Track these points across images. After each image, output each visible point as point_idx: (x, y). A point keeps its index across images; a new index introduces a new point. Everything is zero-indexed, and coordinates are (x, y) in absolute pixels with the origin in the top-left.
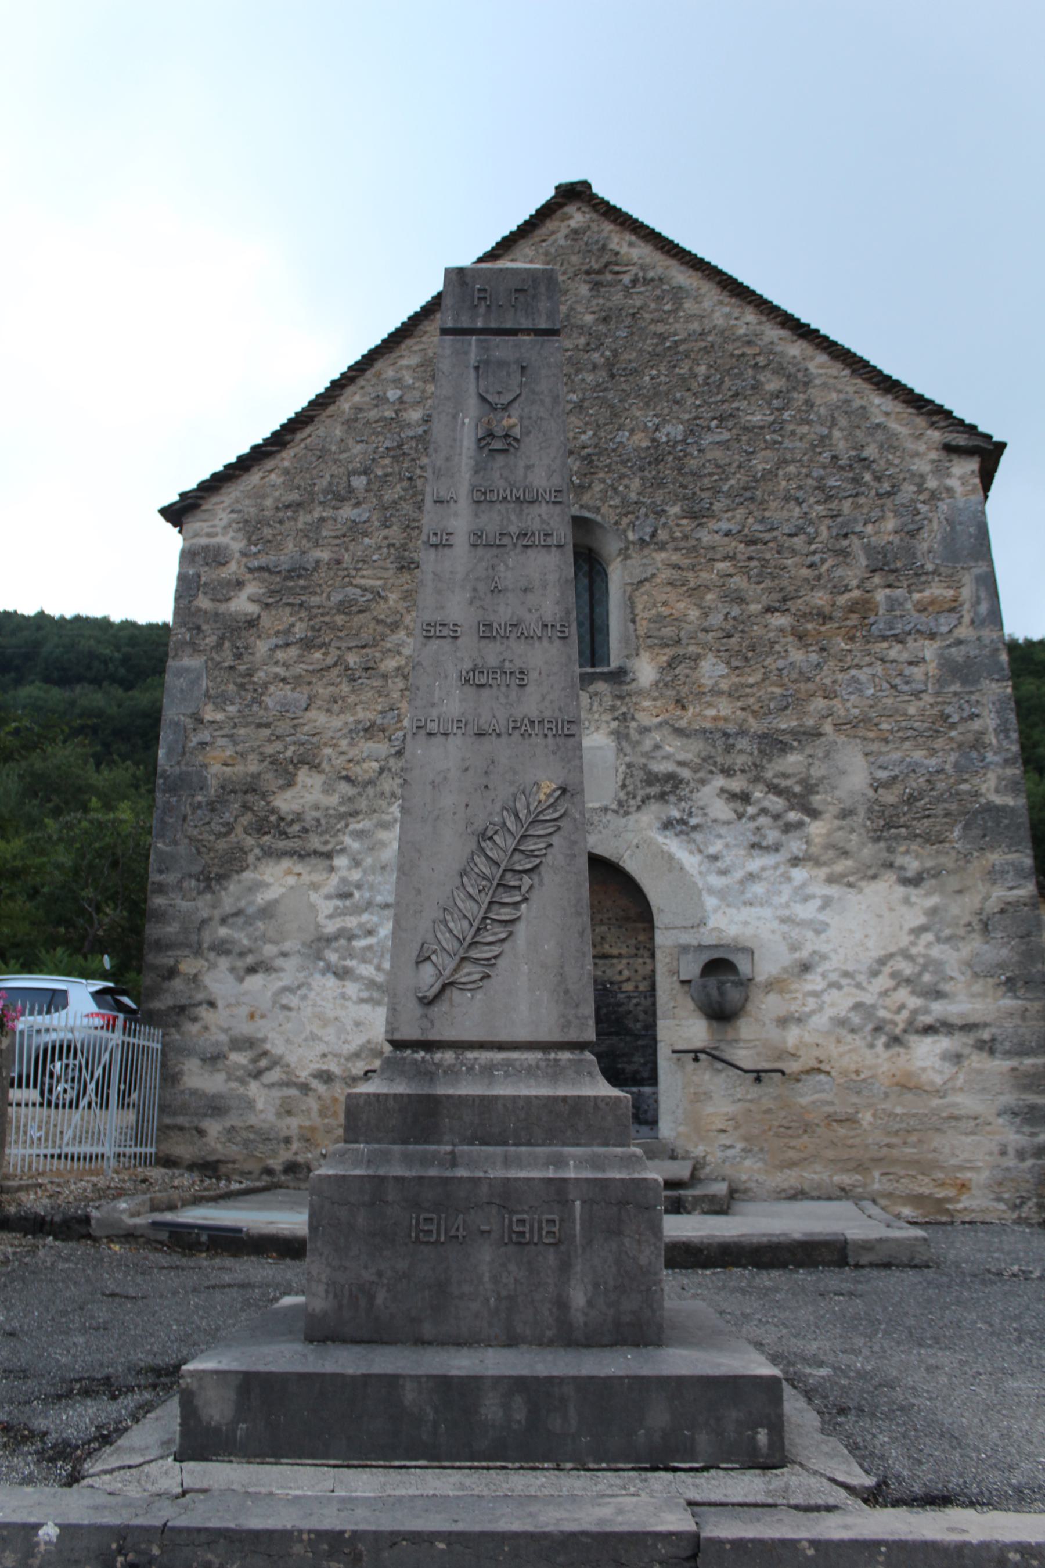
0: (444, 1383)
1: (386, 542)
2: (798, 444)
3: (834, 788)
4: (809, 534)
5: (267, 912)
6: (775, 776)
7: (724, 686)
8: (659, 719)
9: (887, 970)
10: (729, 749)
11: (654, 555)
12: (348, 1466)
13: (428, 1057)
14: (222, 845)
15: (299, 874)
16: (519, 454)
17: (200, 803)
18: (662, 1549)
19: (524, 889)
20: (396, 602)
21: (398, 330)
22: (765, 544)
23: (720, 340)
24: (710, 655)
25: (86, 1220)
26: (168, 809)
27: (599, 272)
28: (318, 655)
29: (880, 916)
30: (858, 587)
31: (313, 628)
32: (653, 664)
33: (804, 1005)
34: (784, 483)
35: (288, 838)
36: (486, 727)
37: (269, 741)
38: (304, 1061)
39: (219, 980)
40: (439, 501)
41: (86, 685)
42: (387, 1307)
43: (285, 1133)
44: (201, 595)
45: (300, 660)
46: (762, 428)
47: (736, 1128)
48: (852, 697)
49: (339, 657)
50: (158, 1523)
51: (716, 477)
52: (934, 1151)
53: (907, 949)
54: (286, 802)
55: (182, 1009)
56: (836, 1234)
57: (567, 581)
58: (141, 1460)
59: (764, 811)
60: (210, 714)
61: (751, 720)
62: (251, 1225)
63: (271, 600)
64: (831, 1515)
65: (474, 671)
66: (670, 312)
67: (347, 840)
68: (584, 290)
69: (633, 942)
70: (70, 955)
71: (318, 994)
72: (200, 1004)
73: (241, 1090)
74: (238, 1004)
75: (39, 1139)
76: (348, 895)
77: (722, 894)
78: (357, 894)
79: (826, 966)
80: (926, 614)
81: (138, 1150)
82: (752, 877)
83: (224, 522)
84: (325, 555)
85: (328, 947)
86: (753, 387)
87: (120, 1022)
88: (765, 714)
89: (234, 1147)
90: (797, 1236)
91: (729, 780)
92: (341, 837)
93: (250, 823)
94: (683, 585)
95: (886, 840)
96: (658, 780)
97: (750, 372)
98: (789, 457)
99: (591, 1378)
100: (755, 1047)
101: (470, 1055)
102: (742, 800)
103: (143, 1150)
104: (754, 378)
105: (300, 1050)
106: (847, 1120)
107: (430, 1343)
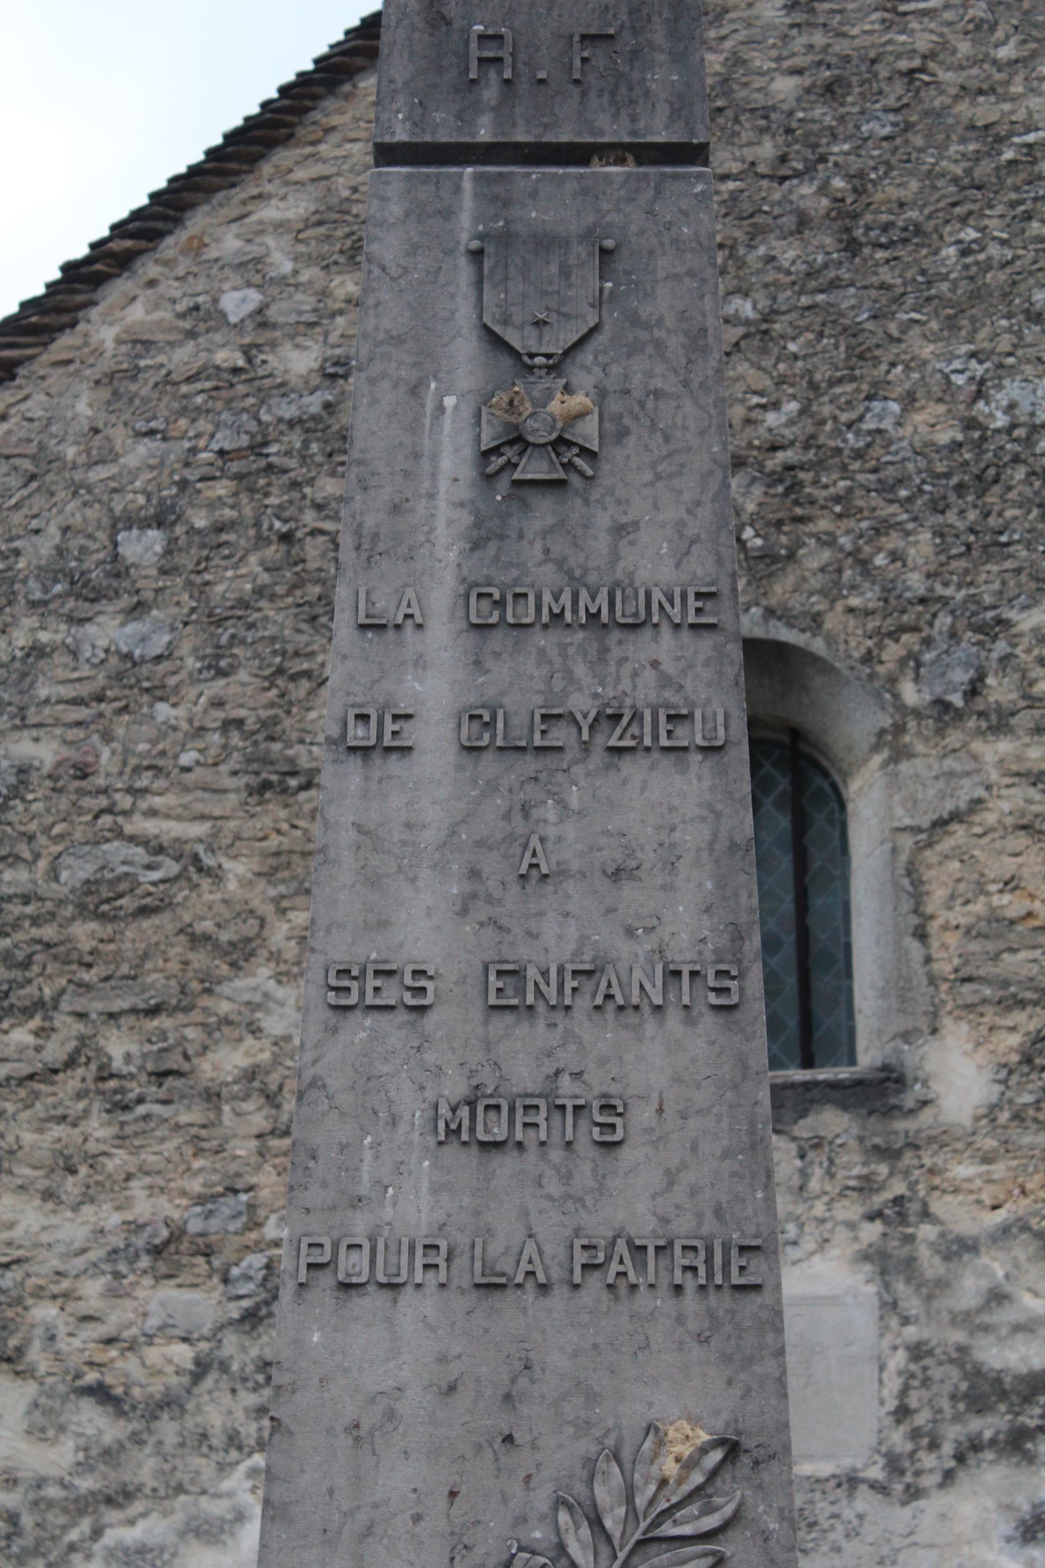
1: (220, 714)
8: (1000, 1216)
11: (977, 746)
16: (595, 494)
20: (246, 884)
21: (251, 124)
28: (21, 1035)
36: (505, 1265)
49: (82, 1039)
65: (472, 1104)
84: (44, 752)
96: (1004, 1395)
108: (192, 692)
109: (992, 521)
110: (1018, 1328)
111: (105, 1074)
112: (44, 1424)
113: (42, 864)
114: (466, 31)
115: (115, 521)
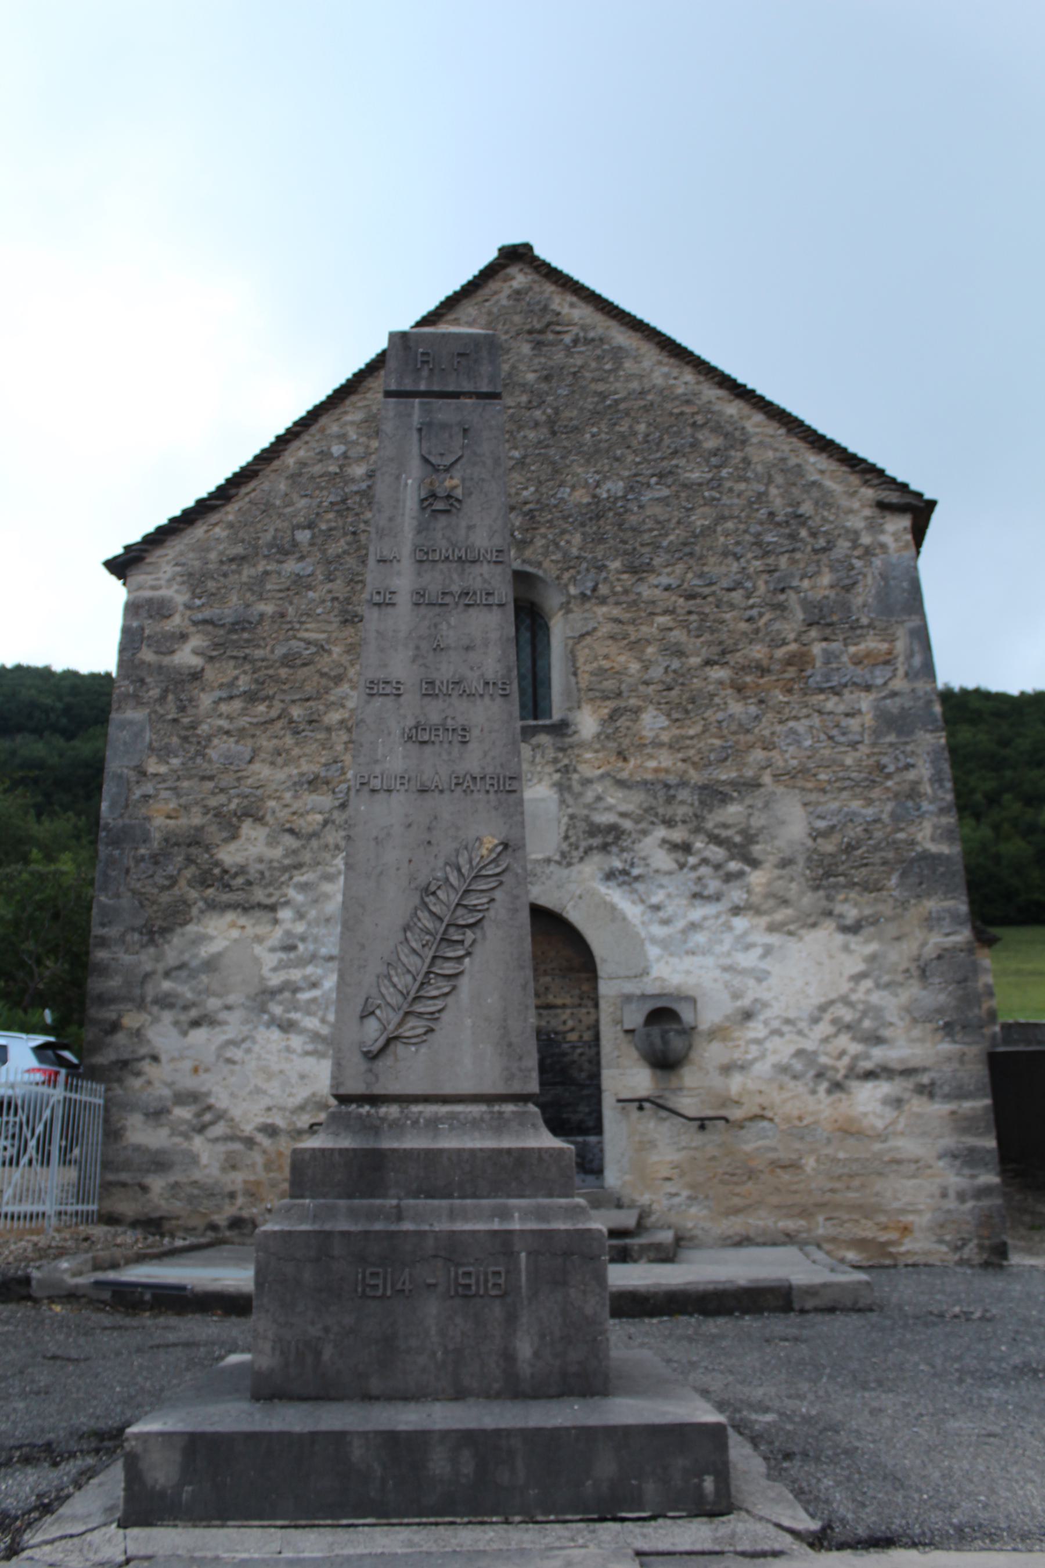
0: (392, 1439)
3: (774, 838)
4: (746, 589)
5: (211, 965)
6: (716, 826)
7: (665, 737)
9: (828, 1016)
11: (595, 609)
12: (296, 1527)
13: (373, 1111)
14: (165, 898)
17: (143, 856)
19: (467, 943)
20: (340, 655)
22: (705, 598)
24: (651, 708)
25: (27, 1280)
26: (111, 862)
27: (541, 332)
28: (262, 708)
29: (820, 964)
30: (796, 640)
34: (722, 539)
35: (231, 890)
36: (428, 783)
38: (249, 1115)
39: (162, 1034)
40: (382, 561)
43: (230, 1188)
44: (144, 648)
45: (244, 712)
46: (700, 484)
48: (791, 749)
51: (655, 533)
54: (229, 855)
58: (83, 1528)
59: (705, 861)
60: (153, 766)
63: (214, 653)
66: (610, 371)
68: (526, 349)
69: (577, 992)
72: (143, 1058)
74: (182, 1058)
76: (292, 948)
77: (664, 944)
78: (301, 947)
79: (768, 1013)
83: (168, 575)
84: (269, 608)
85: (272, 1000)
86: (692, 445)
88: (706, 766)
89: (178, 1204)
90: (742, 1282)
91: (670, 831)
92: (285, 890)
93: (194, 876)
94: (624, 638)
95: (825, 888)
96: (600, 832)
97: (689, 430)
98: (727, 513)
101: (415, 1109)
104: (693, 436)
106: (791, 1166)
107: (377, 1398)
111: (291, 721)
112: (272, 841)
113: (268, 648)
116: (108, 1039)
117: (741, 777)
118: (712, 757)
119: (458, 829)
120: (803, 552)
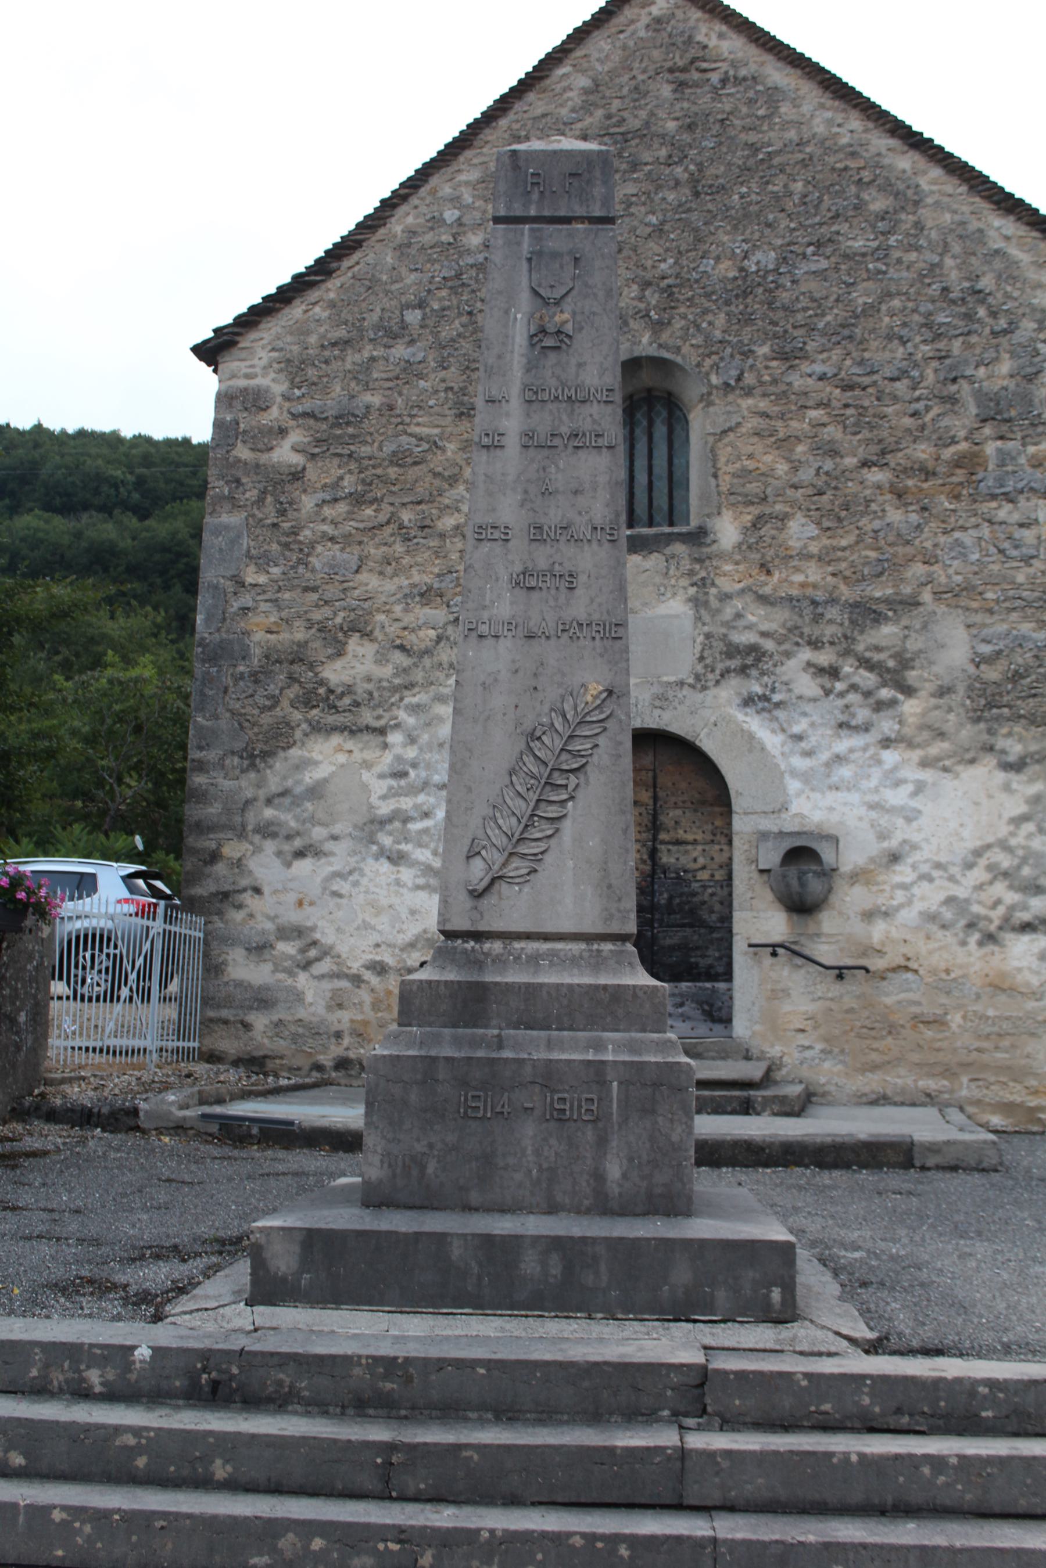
0: (488, 1241)
1: (444, 385)
2: (905, 274)
3: (931, 663)
4: (913, 378)
5: (315, 792)
6: (867, 649)
7: (814, 548)
9: (983, 862)
10: (817, 618)
11: (739, 401)
12: (401, 1312)
13: (477, 946)
14: (266, 719)
15: (351, 751)
16: (571, 351)
17: (242, 674)
18: (675, 1378)
19: (570, 788)
20: (454, 453)
22: (864, 389)
23: (819, 152)
24: (799, 515)
25: (135, 1112)
26: (208, 680)
27: (684, 70)
28: (369, 512)
29: (977, 804)
30: (966, 439)
31: (363, 481)
32: (736, 524)
33: (892, 898)
34: (887, 319)
35: (338, 712)
36: (535, 630)
37: (317, 606)
38: (356, 951)
39: (265, 865)
40: (491, 401)
41: (94, 513)
42: (437, 1176)
43: (336, 1027)
44: (239, 444)
45: (350, 516)
46: (864, 255)
47: (815, 1028)
48: (956, 563)
49: (392, 513)
50: (237, 1348)
51: (811, 312)
52: (1028, 1057)
53: (1006, 840)
54: (335, 673)
55: (226, 895)
56: (903, 1136)
57: (617, 483)
58: (216, 1304)
59: (854, 687)
60: (251, 576)
61: (843, 587)
62: (303, 1118)
63: (317, 450)
64: (830, 1359)
65: (524, 574)
66: (764, 117)
67: (402, 715)
68: (667, 91)
69: (710, 827)
70: (90, 833)
71: (371, 880)
72: (245, 890)
73: (290, 981)
74: (286, 890)
75: (74, 1033)
76: (404, 774)
77: (806, 777)
78: (412, 774)
79: (917, 856)
80: (1041, 469)
81: (181, 1044)
82: (839, 759)
83: (264, 362)
84: (375, 400)
85: (381, 830)
86: (856, 208)
87: (160, 910)
88: (858, 581)
89: (282, 1042)
90: (863, 1136)
91: (817, 653)
92: (395, 712)
93: (297, 696)
94: (771, 435)
95: (987, 721)
96: (739, 652)
97: (853, 189)
98: (893, 289)
99: (621, 1239)
100: (837, 942)
101: (517, 945)
102: (830, 674)
103: (186, 1044)
104: (858, 197)
105: (352, 940)
106: (935, 1021)
107: (477, 1210)
108: (433, 376)
109: (749, 310)
110: (746, 628)
111: (401, 527)
112: (381, 659)
114: (527, 172)
115: (402, 306)
116: (207, 870)
117: (897, 594)
118: (866, 572)
119: (564, 675)
120: (980, 335)
